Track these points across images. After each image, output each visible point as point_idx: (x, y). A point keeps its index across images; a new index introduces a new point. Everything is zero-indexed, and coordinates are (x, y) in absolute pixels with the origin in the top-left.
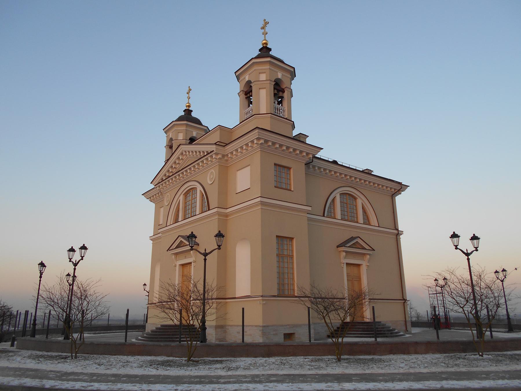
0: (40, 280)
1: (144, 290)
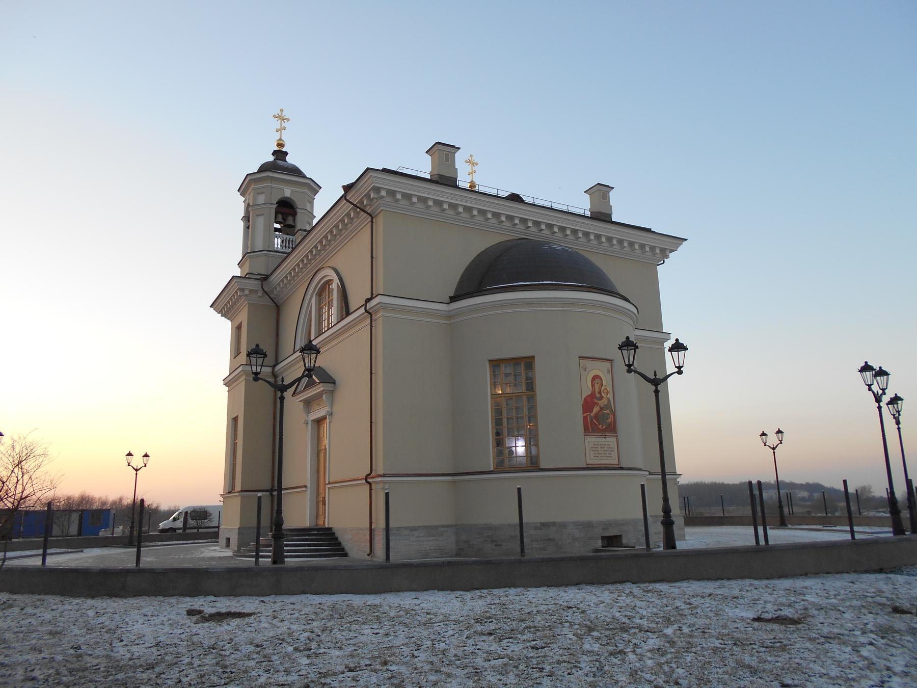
0: (899, 429)
1: (129, 465)
